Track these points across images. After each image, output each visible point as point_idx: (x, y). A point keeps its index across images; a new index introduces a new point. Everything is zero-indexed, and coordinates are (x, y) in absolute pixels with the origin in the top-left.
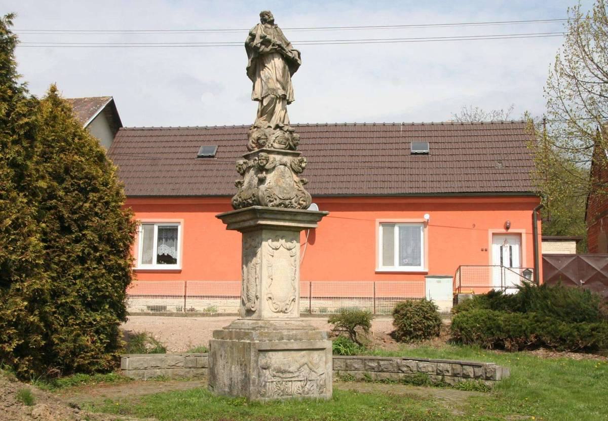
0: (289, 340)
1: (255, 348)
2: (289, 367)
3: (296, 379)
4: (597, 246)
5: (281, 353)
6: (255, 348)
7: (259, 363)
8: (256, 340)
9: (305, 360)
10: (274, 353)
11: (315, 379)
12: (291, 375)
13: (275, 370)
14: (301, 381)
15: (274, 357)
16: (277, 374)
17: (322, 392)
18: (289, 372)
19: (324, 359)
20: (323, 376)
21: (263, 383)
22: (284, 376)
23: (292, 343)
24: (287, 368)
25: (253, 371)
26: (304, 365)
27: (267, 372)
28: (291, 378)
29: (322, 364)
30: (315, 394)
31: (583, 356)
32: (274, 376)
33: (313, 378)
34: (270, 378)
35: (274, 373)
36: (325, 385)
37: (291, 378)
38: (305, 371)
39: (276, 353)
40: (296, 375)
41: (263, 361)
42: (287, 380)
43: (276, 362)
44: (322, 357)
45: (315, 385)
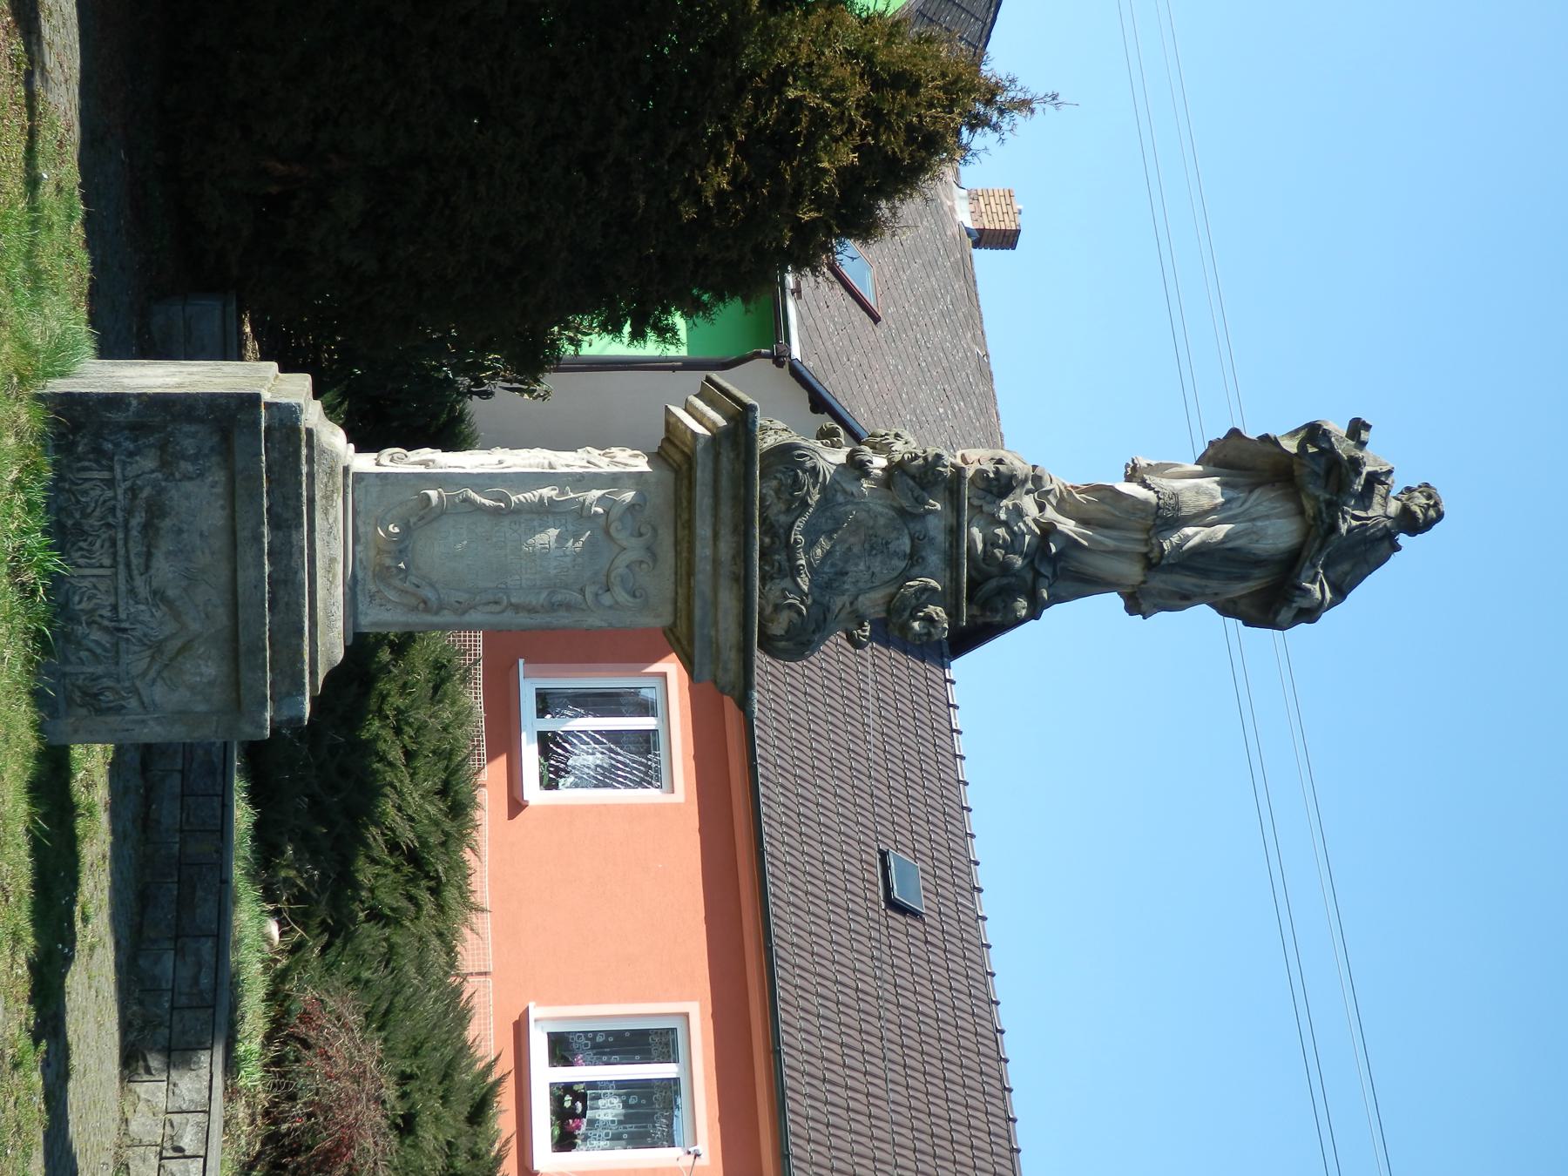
18: (149, 556)
27: (148, 463)
32: (133, 491)
40: (139, 582)
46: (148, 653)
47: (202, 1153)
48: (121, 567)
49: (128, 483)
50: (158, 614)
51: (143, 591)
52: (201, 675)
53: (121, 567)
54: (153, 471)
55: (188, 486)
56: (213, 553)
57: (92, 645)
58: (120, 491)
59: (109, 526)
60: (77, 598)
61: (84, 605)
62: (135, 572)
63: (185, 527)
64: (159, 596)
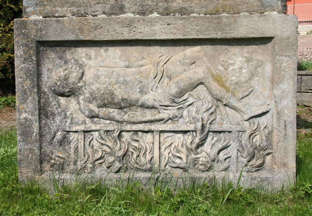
0: (143, 13)
1: (26, 36)
2: (142, 92)
3: (169, 126)
4: (172, 117)
5: (115, 52)
6: (26, 36)
7: (45, 78)
8: (34, 13)
9: (199, 72)
10: (92, 51)
11: (234, 128)
12: (149, 115)
13: (92, 98)
14: (185, 132)
15: (91, 63)
16: (103, 111)
17: (260, 167)
18: (143, 106)
19: (268, 68)
20: (263, 120)
21: (59, 135)
22: (126, 117)
23: (152, 22)
24: (135, 95)
25: (24, 101)
26: (194, 86)
27: (71, 105)
28: (151, 122)
29: (260, 86)
30: (236, 174)
31: (265, 46)
32: (93, 116)
33: (226, 127)
34: (81, 122)
35: (93, 107)
36: (270, 144)
37: (151, 122)
38: (200, 101)
39: (102, 50)
40: (164, 114)
41: (54, 71)
42: (135, 127)
43: (98, 77)
44: (261, 64)
45: (234, 146)
46: (222, 108)
47: (302, 91)
48: (153, 127)
49: (88, 120)
50: (191, 100)
51: (171, 112)
52: (241, 68)
53: (153, 127)
54: (79, 103)
55: (88, 76)
56: (143, 58)
57: (216, 150)
58: (94, 127)
59: (120, 136)
60: (178, 161)
61: (183, 156)
62: (157, 117)
63: (121, 79)
64: (177, 98)
